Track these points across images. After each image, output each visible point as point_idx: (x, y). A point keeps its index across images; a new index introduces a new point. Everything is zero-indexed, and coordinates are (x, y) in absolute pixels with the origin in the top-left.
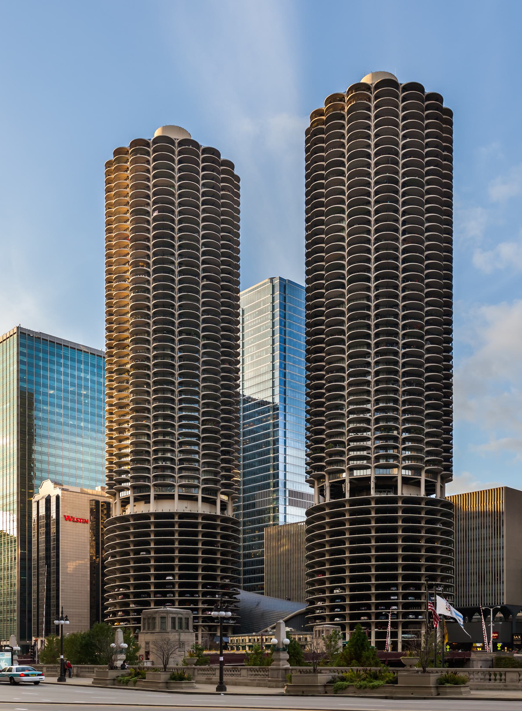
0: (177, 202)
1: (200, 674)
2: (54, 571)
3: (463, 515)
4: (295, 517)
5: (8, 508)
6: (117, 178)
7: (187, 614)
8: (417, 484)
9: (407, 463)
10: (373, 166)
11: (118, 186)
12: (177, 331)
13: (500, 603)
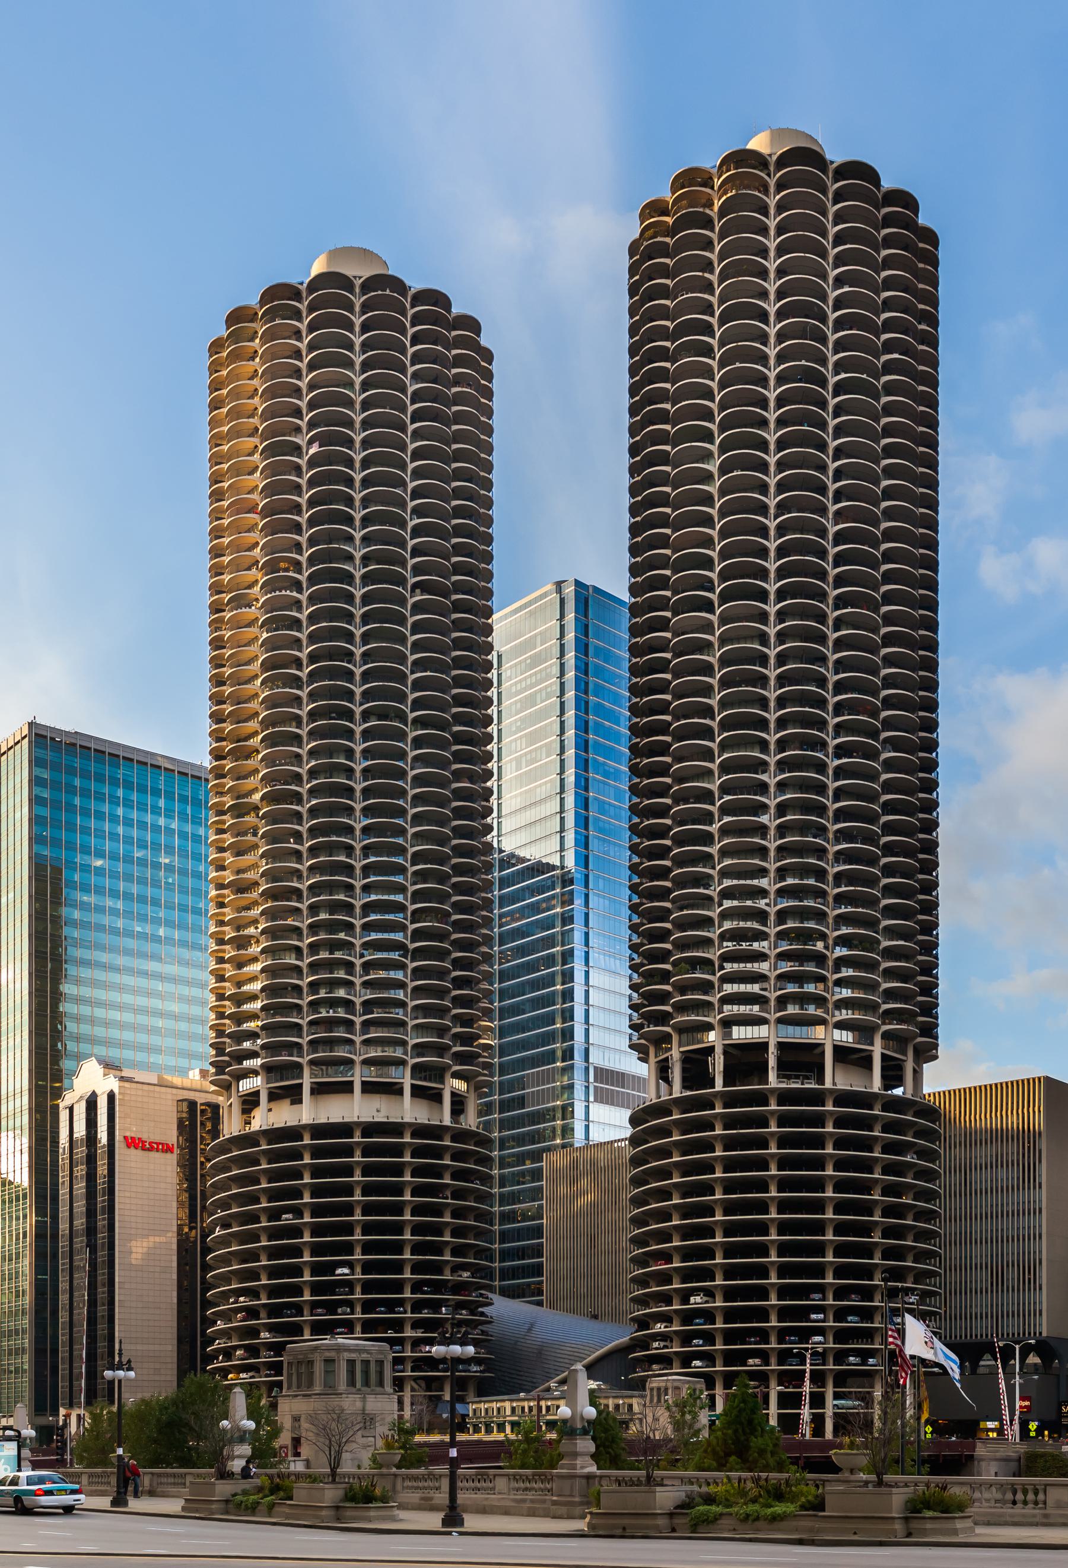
0: (358, 419)
1: (408, 1487)
2: (103, 1261)
3: (960, 1135)
4: (607, 1128)
5: (11, 1123)
6: (232, 377)
7: (380, 1352)
8: (864, 1062)
9: (845, 1015)
10: (772, 340)
11: (235, 394)
12: (358, 710)
13: (1035, 1333)
